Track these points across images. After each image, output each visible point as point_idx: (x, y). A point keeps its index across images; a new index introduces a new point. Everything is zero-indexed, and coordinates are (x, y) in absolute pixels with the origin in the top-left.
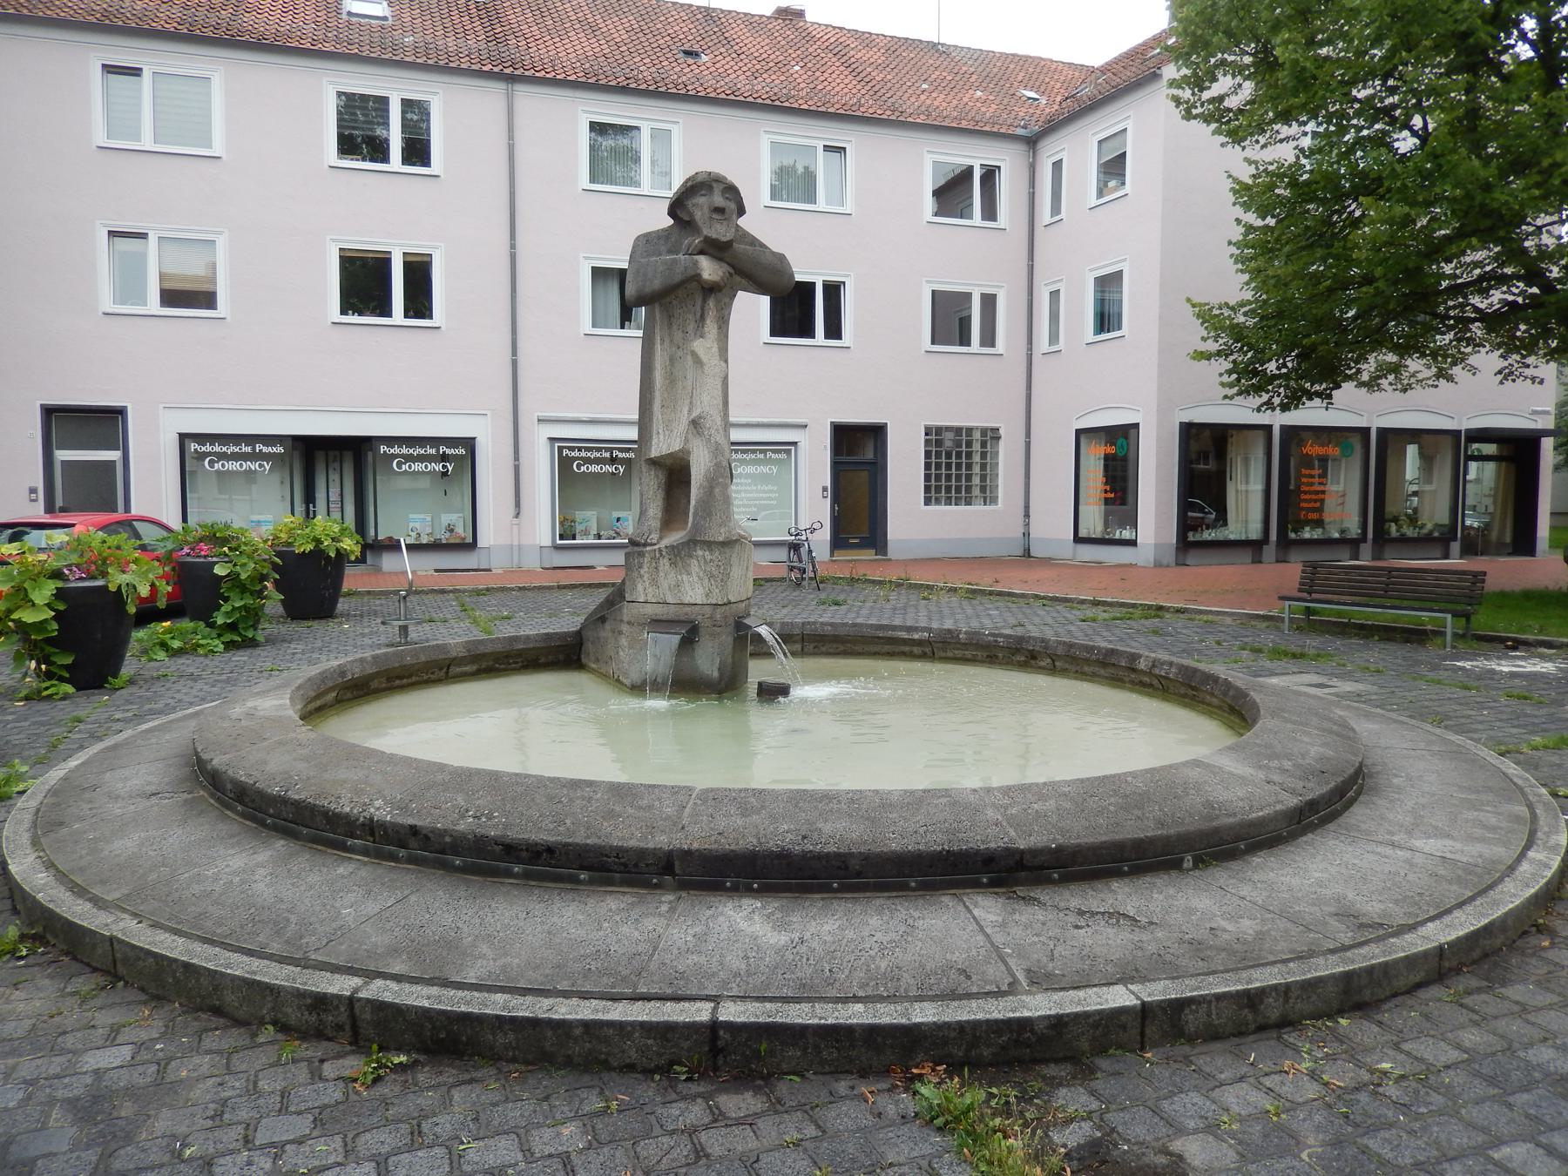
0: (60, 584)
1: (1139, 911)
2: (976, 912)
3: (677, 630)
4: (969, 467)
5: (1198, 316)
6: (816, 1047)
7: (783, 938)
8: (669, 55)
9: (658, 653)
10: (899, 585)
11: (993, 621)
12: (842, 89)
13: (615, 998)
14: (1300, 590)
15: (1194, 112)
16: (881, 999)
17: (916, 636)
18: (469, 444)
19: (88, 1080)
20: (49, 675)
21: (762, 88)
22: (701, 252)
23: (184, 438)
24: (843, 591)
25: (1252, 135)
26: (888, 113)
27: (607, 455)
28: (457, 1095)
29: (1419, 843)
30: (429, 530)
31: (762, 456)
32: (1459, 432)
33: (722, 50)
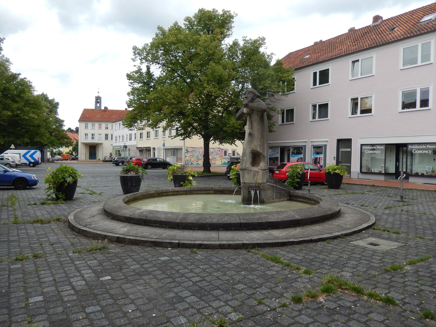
23: (362, 145)
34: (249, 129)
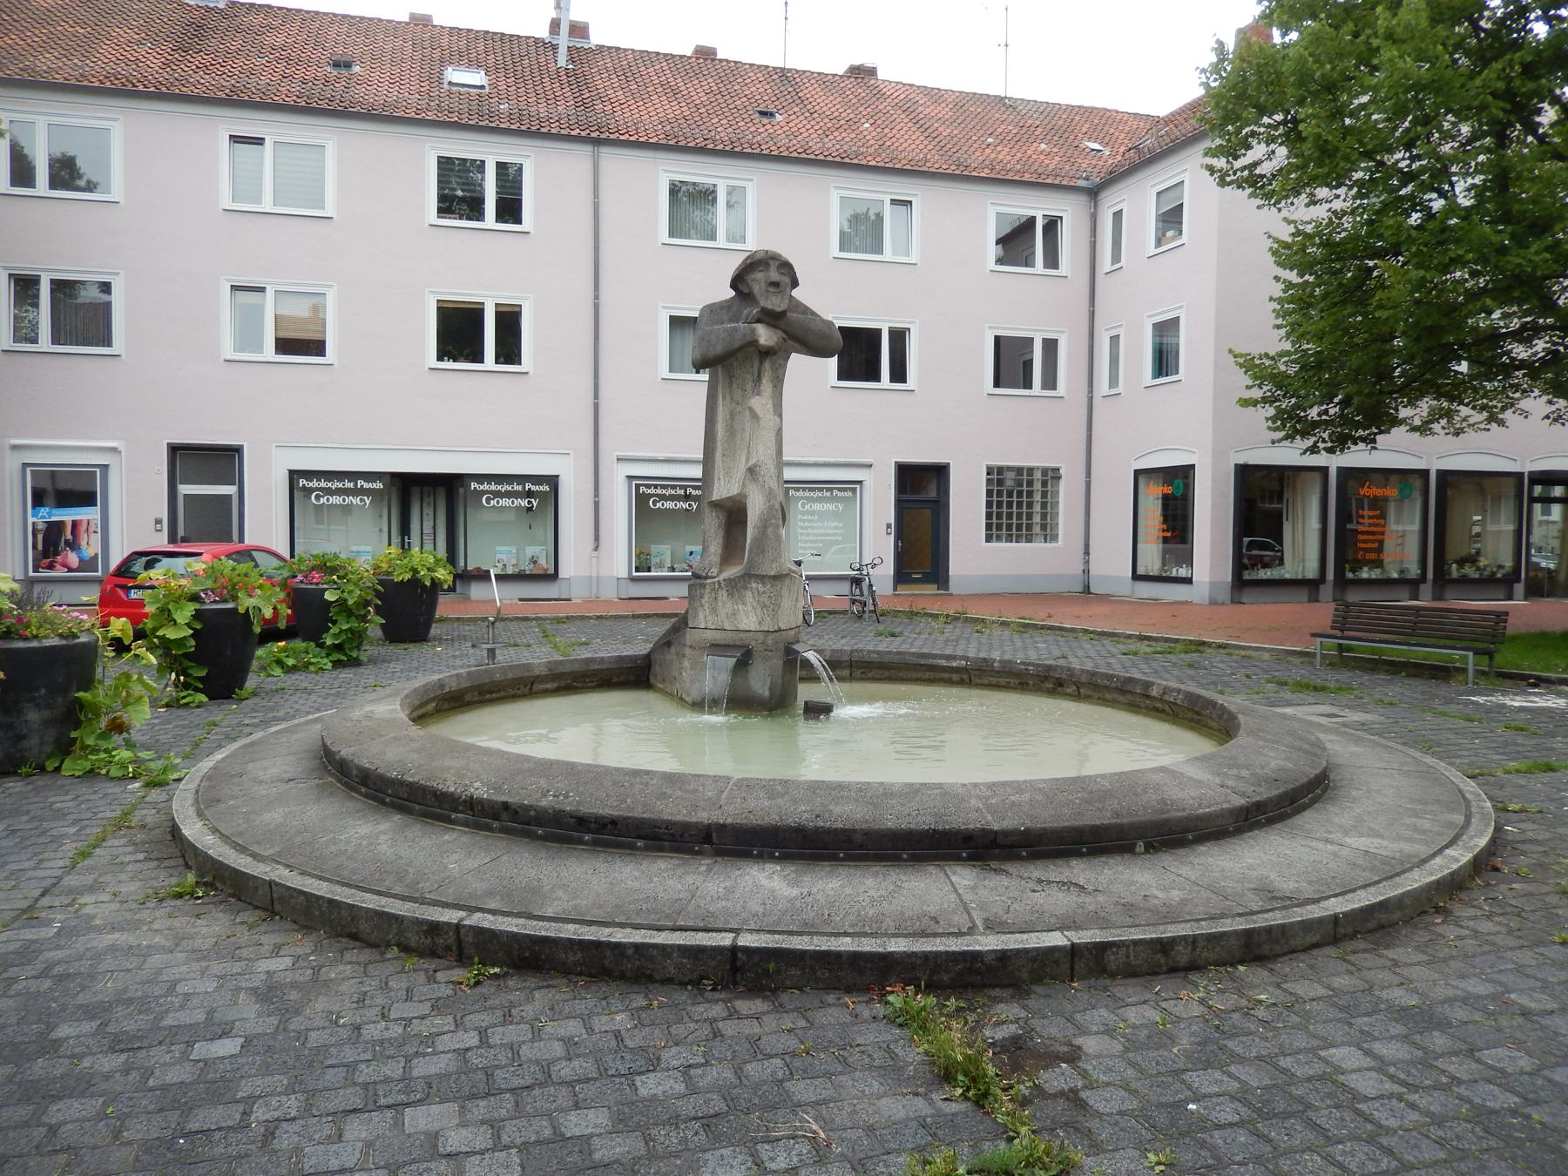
0: (198, 606)
1: (1088, 881)
2: (953, 878)
3: (734, 653)
4: (1030, 505)
5: (1241, 366)
6: (812, 968)
7: (795, 892)
8: (746, 116)
9: (715, 675)
10: (956, 619)
11: (1037, 652)
12: (909, 145)
13: (659, 929)
14: (1333, 628)
15: (1228, 179)
16: (865, 935)
17: (954, 664)
18: (553, 481)
19: (264, 977)
20: (186, 686)
21: (831, 146)
22: (758, 321)
23: (294, 475)
24: (901, 623)
25: (1287, 197)
26: (953, 167)
27: (682, 492)
28: (537, 995)
29: (1349, 840)
30: (514, 561)
31: (828, 494)
32: (1523, 474)
33: (796, 109)
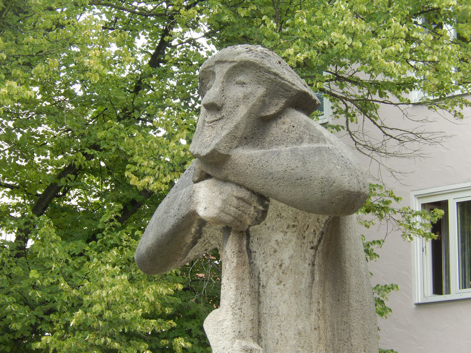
34: (240, 335)
